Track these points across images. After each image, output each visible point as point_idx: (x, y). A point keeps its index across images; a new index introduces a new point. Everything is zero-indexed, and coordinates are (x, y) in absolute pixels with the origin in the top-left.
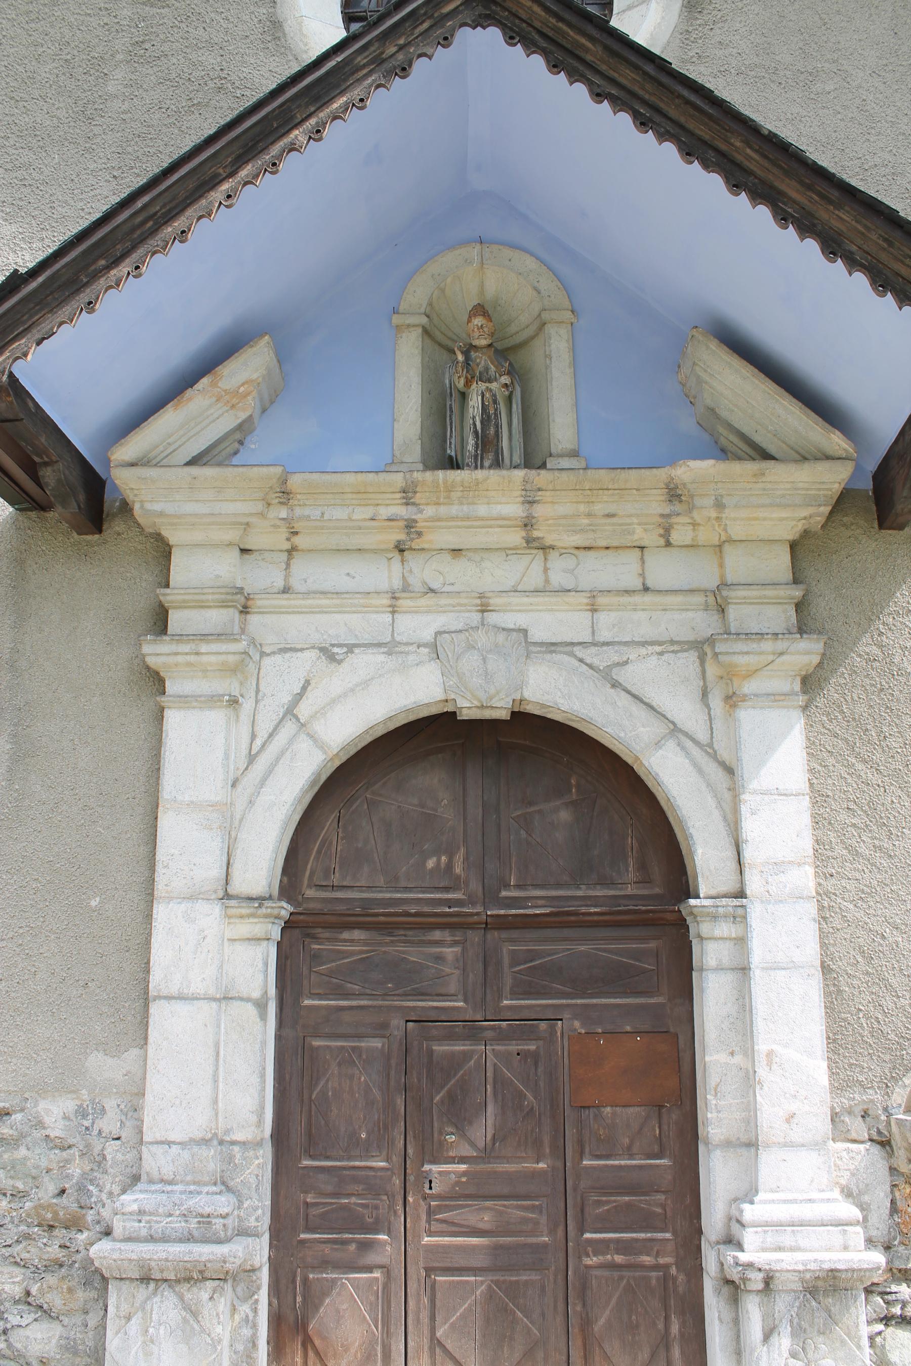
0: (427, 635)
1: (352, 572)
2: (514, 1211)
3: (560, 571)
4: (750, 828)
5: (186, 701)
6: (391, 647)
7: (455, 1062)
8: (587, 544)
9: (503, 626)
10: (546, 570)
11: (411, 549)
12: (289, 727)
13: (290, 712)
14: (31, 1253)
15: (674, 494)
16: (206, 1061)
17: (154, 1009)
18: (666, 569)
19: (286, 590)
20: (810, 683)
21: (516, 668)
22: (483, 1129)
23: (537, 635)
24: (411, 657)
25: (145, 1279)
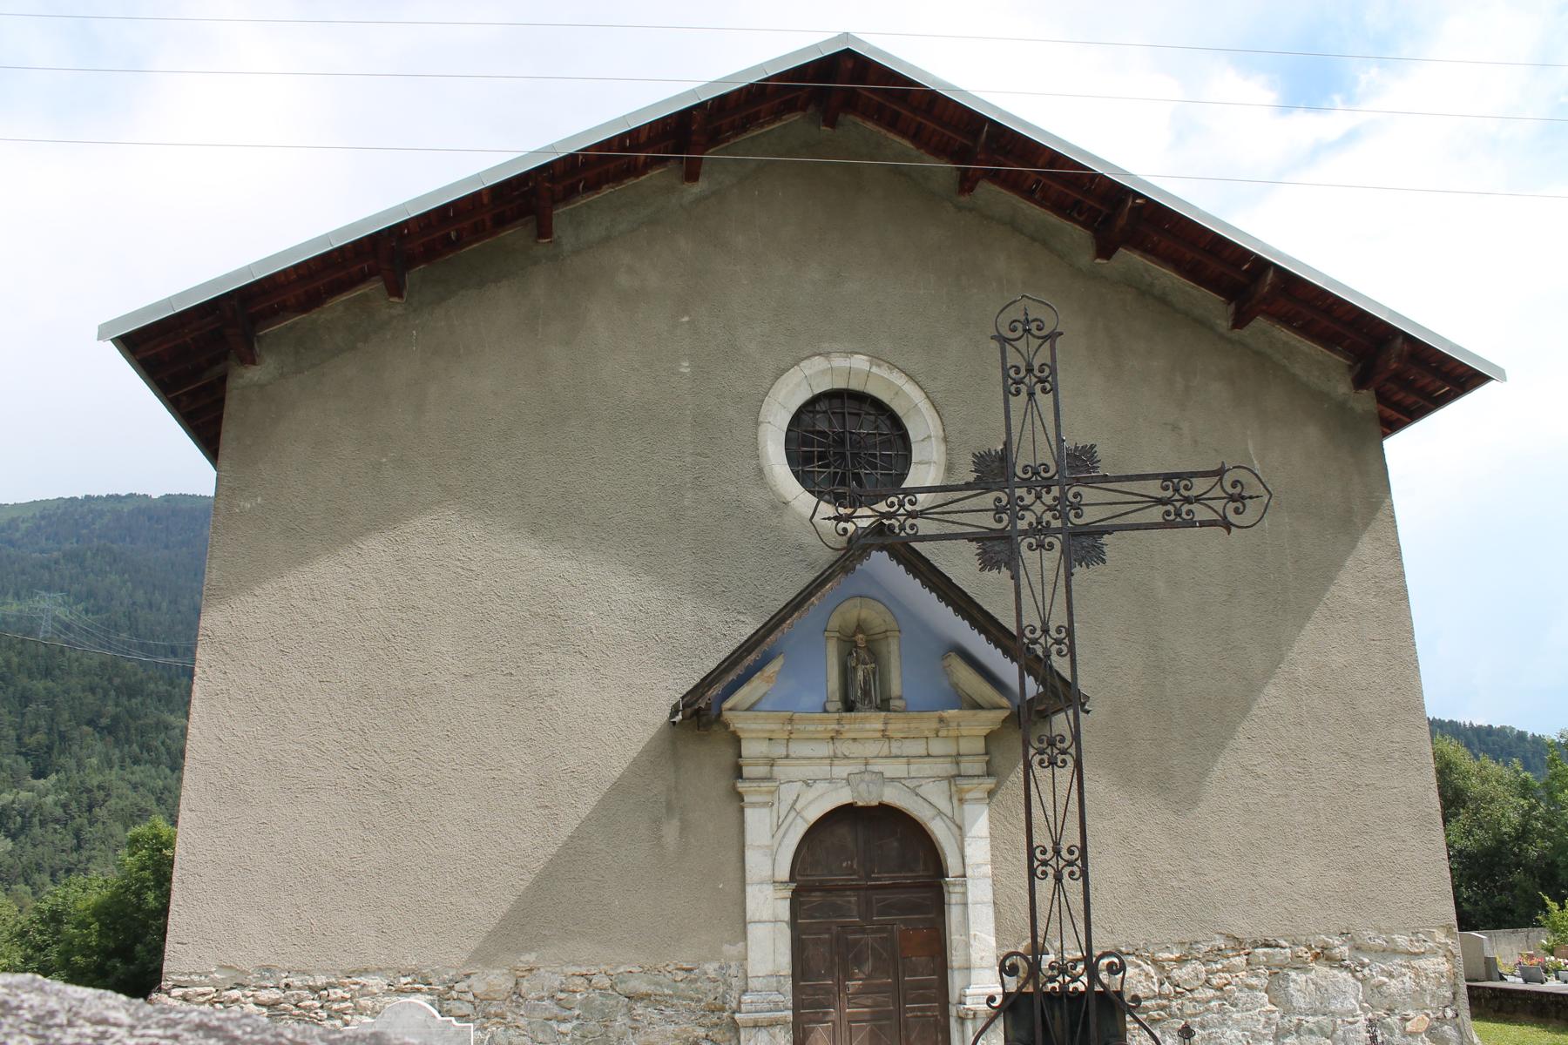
2: (880, 998)
4: (968, 851)
5: (754, 805)
6: (831, 780)
7: (857, 942)
12: (793, 814)
13: (792, 807)
14: (706, 1021)
15: (941, 720)
16: (768, 948)
17: (750, 927)
18: (937, 747)
19: (787, 757)
20: (991, 794)
22: (868, 967)
23: (887, 775)
25: (755, 1027)
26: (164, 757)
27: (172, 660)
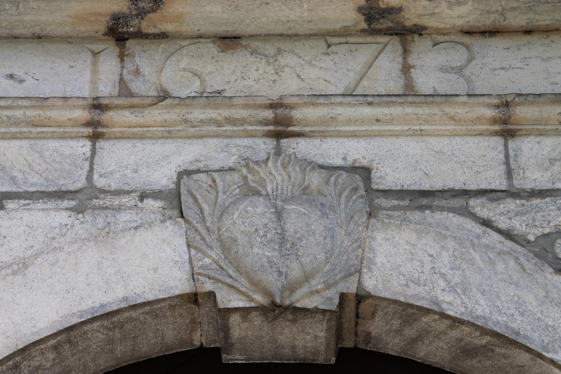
0: (163, 177)
1: (20, 73)
3: (431, 68)
6: (84, 199)
8: (488, 21)
9: (320, 161)
10: (406, 69)
11: (140, 35)
21: (348, 234)
23: (389, 176)
24: (124, 217)
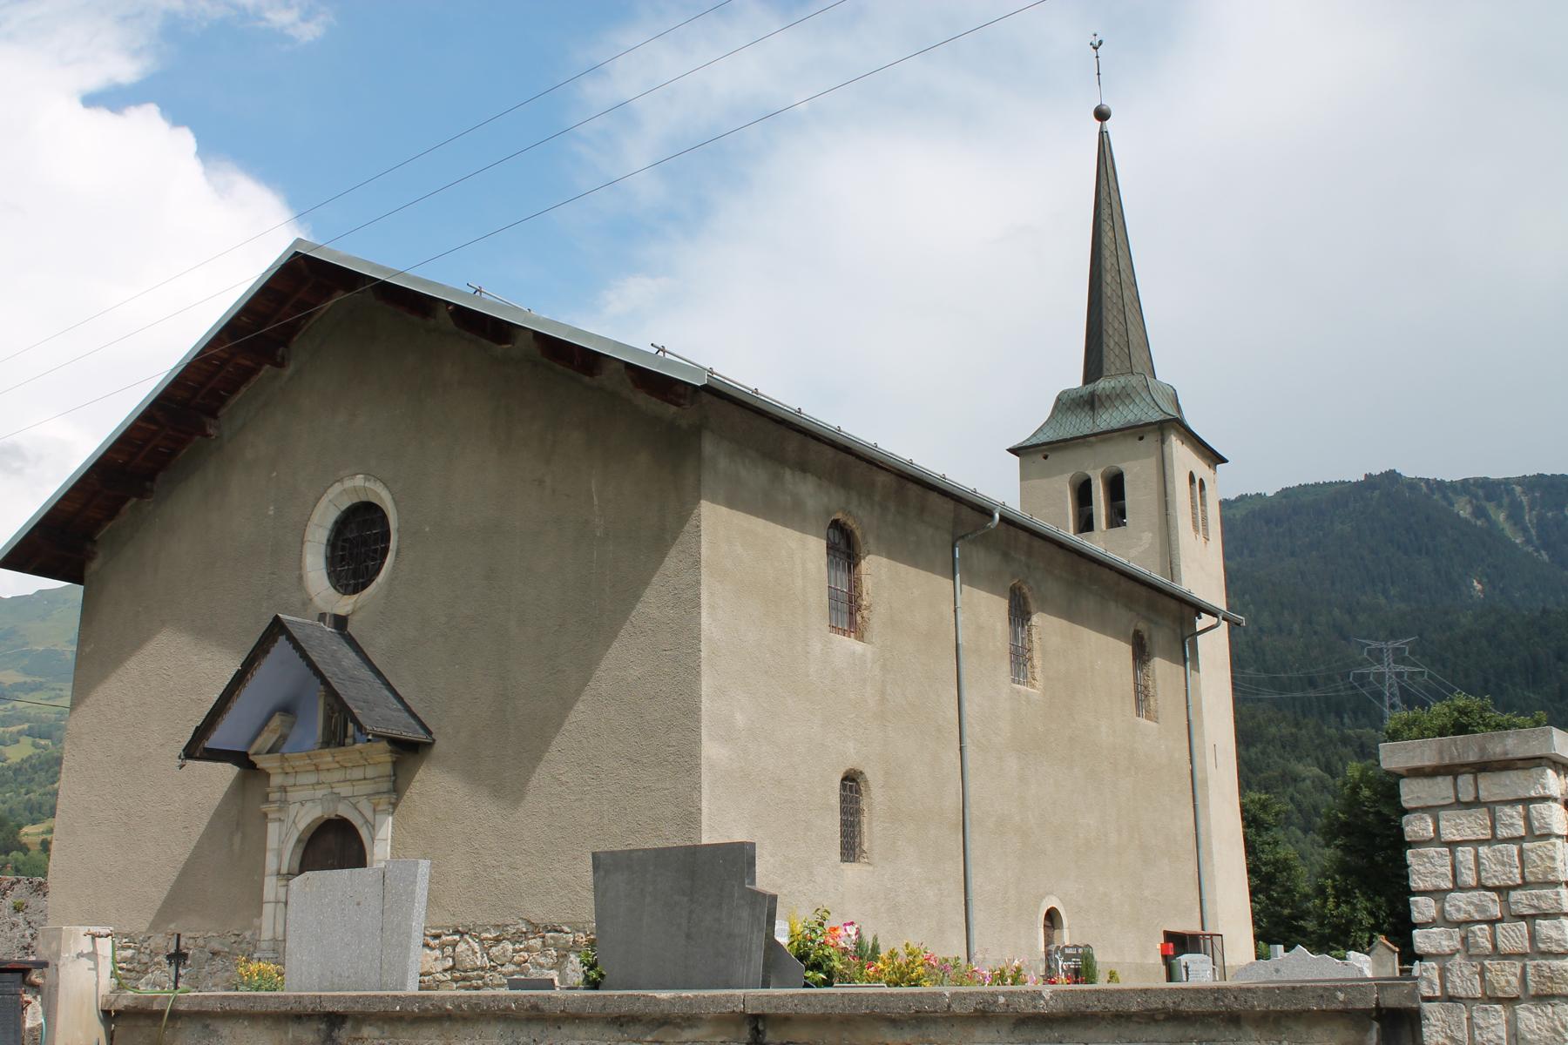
26: (1296, 817)
27: (1312, 694)
